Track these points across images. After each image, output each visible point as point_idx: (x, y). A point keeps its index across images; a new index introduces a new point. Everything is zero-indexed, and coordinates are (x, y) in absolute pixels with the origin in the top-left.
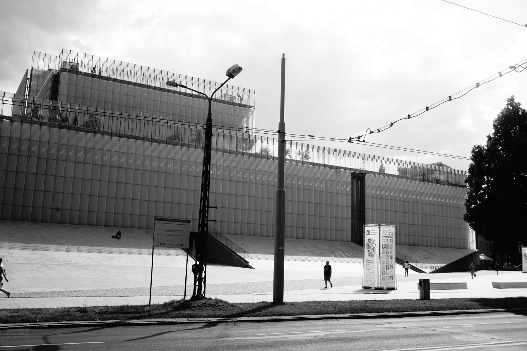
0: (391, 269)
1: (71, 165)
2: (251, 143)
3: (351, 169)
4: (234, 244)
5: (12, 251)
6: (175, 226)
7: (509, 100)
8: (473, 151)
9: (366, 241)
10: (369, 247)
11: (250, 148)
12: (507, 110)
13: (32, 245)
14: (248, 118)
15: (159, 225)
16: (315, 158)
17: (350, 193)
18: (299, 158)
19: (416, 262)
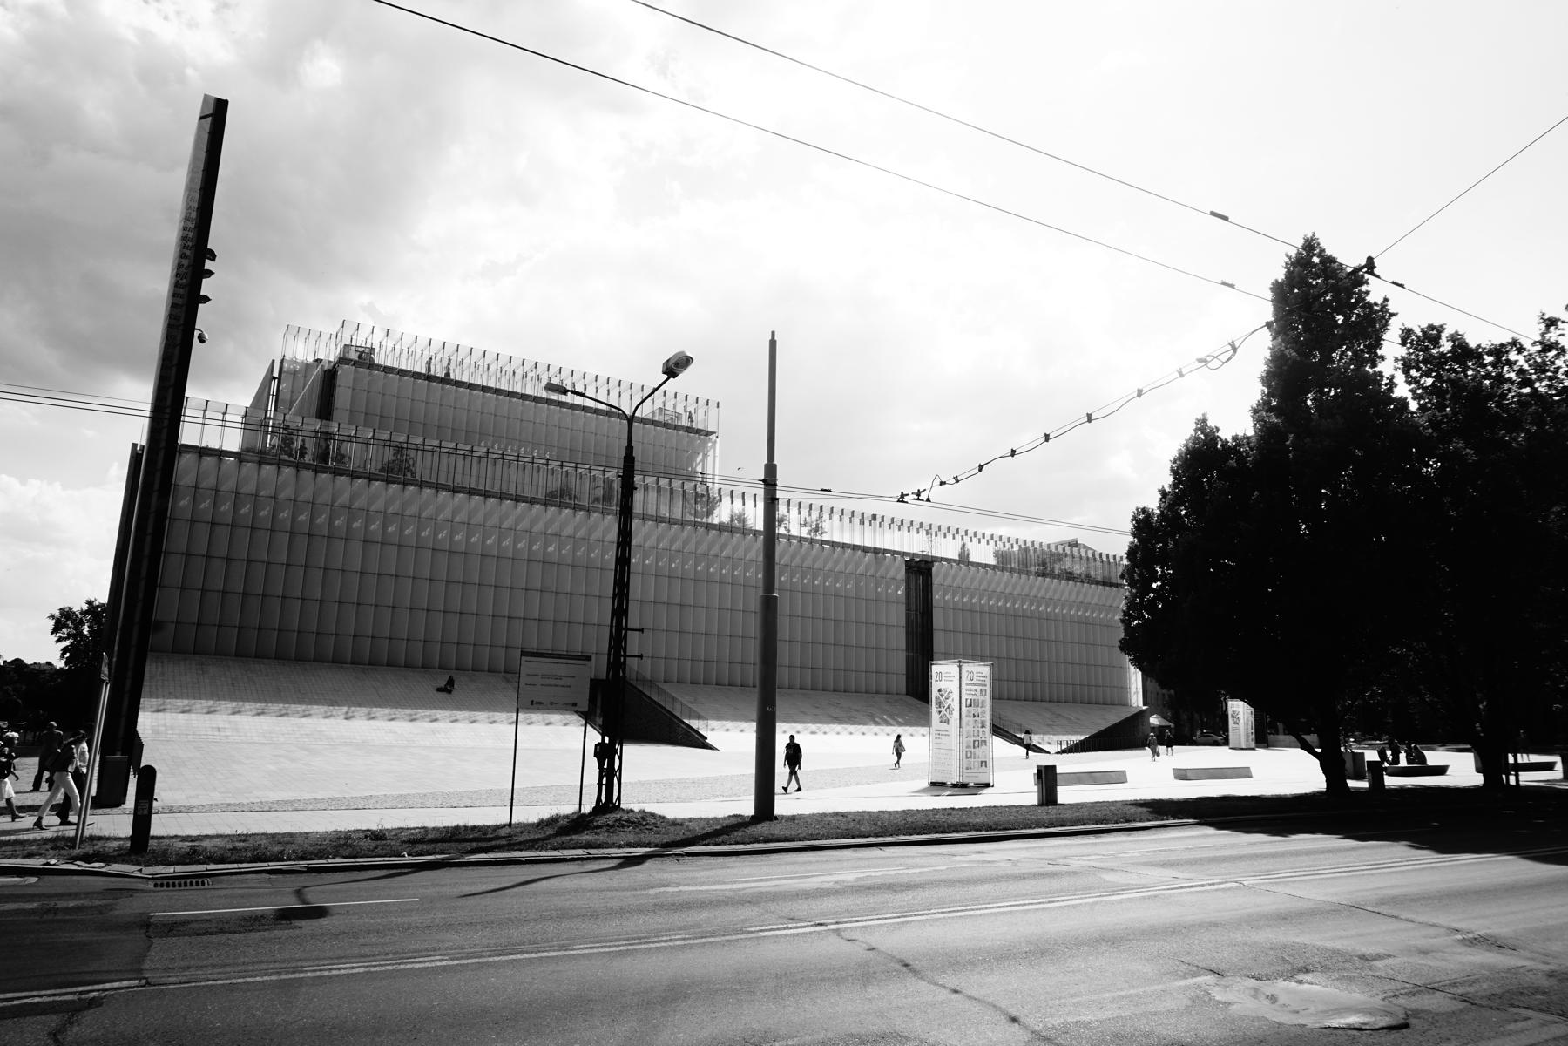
1: (357, 547)
2: (711, 503)
3: (904, 554)
4: (677, 701)
5: (237, 717)
6: (561, 668)
9: (934, 693)
10: (940, 704)
11: (709, 513)
12: (1196, 440)
14: (705, 455)
15: (529, 666)
16: (835, 532)
18: (804, 533)
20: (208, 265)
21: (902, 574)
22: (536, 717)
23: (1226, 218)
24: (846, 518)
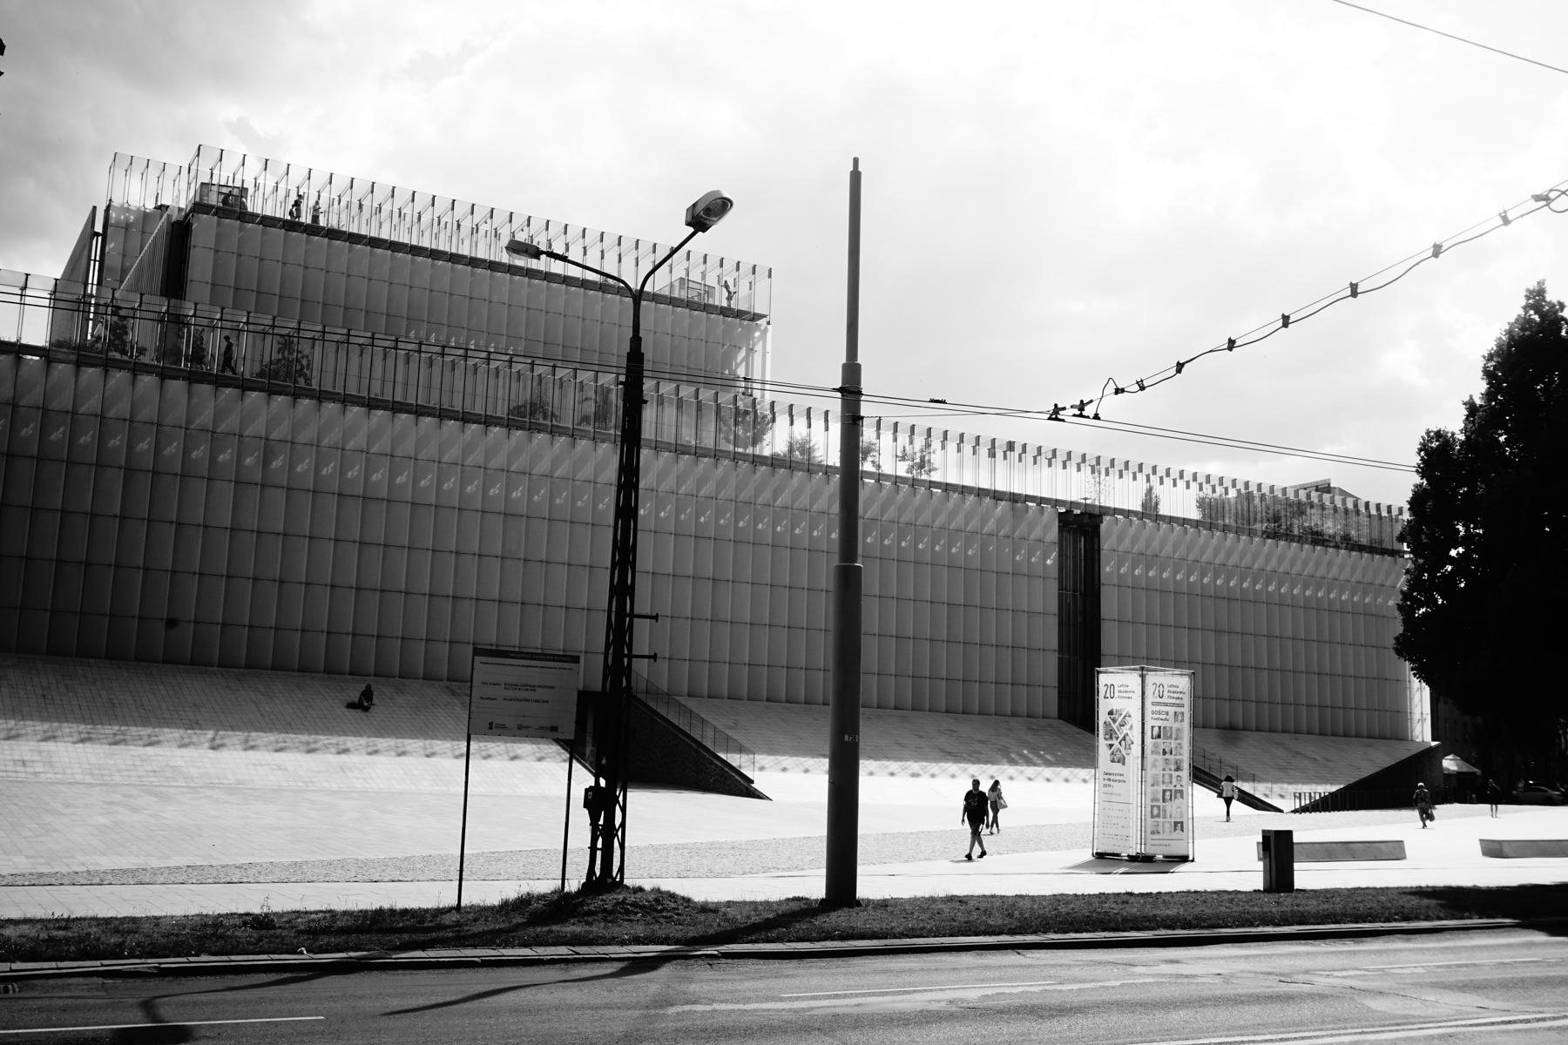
0: (1178, 801)
2: (758, 424)
4: (710, 726)
5: (51, 745)
9: (1103, 717)
14: (751, 351)
16: (949, 468)
17: (1055, 573)
18: (902, 470)
22: (496, 747)
24: (967, 448)
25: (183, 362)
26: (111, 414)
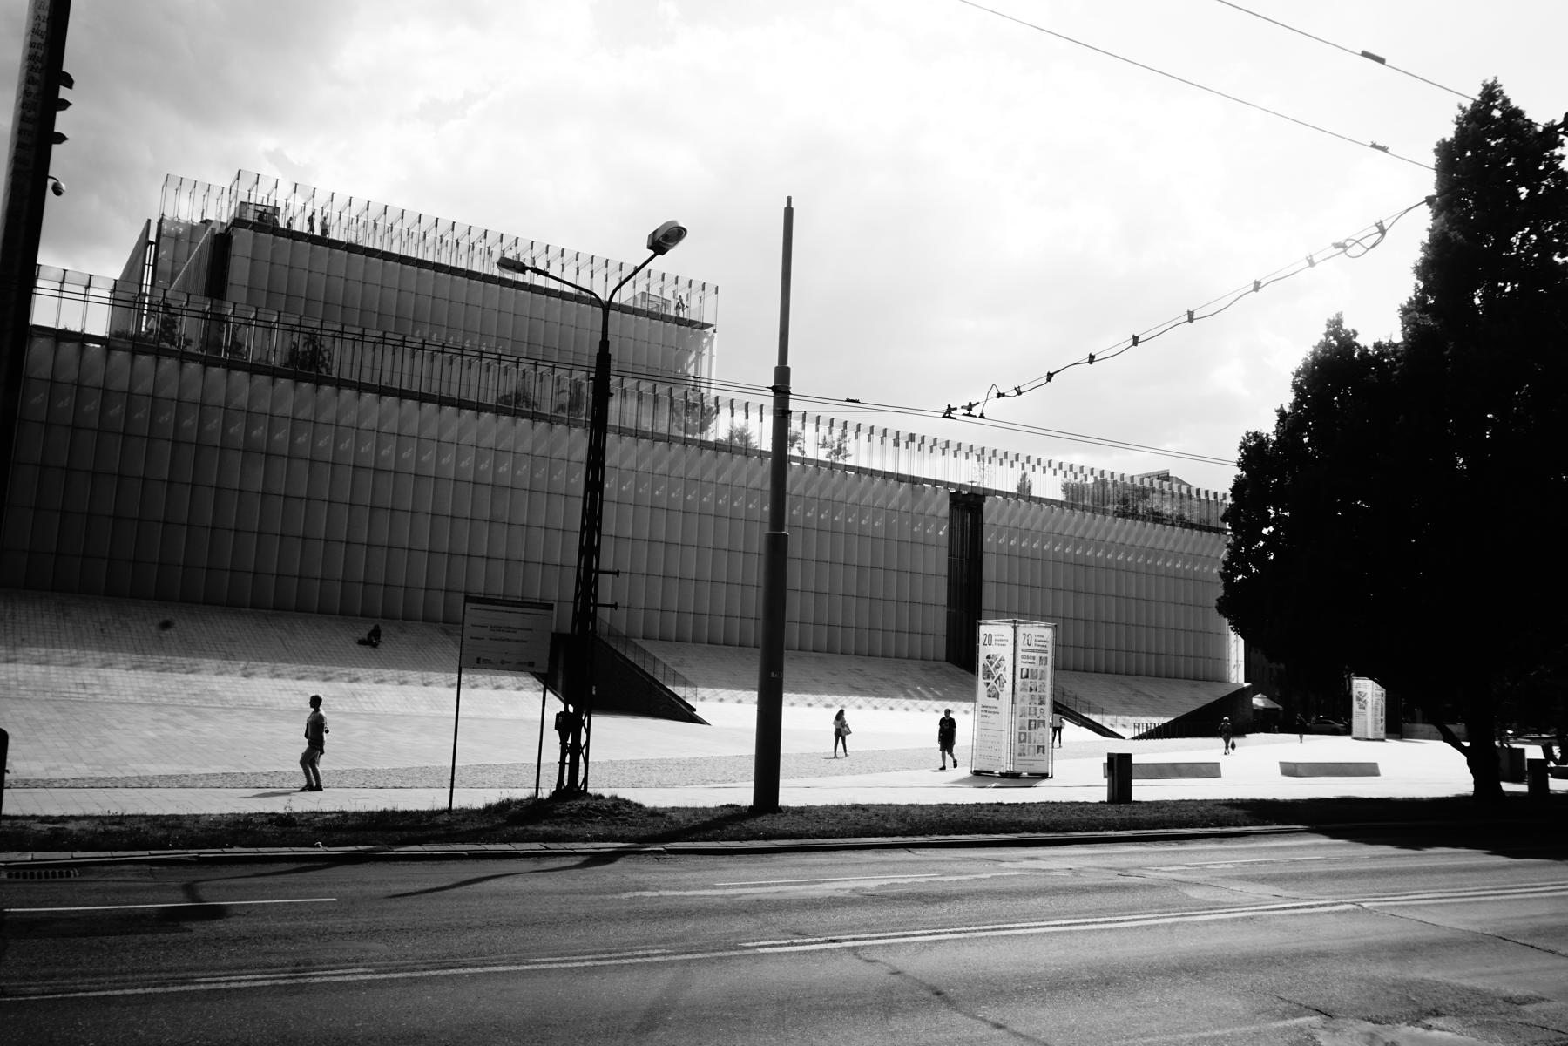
2: (706, 415)
3: (948, 485)
4: (661, 663)
6: (516, 618)
7: (1331, 323)
8: (1244, 446)
9: (982, 660)
10: (988, 674)
12: (1326, 346)
13: (156, 659)
14: (700, 354)
15: (475, 615)
16: (862, 454)
17: (945, 542)
18: (822, 455)
19: (1102, 712)
20: (64, 93)
21: (945, 510)
23: (1381, 61)
25: (218, 352)
26: (138, 390)
